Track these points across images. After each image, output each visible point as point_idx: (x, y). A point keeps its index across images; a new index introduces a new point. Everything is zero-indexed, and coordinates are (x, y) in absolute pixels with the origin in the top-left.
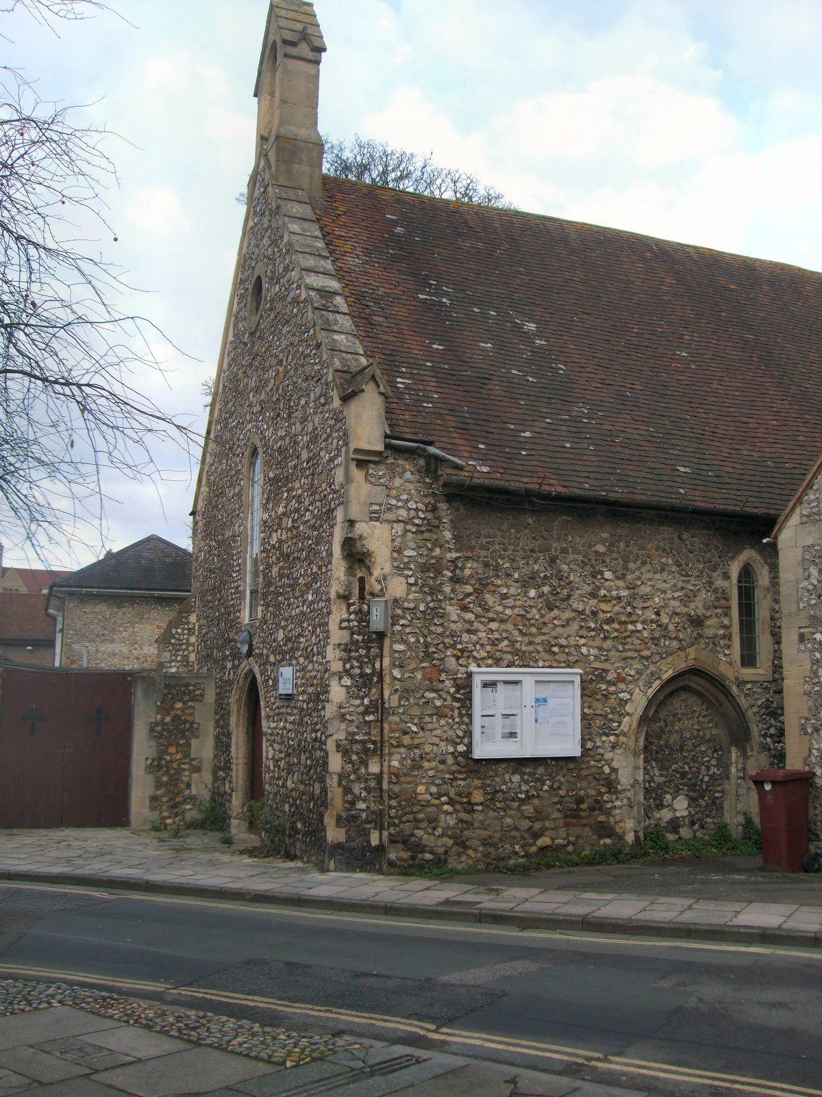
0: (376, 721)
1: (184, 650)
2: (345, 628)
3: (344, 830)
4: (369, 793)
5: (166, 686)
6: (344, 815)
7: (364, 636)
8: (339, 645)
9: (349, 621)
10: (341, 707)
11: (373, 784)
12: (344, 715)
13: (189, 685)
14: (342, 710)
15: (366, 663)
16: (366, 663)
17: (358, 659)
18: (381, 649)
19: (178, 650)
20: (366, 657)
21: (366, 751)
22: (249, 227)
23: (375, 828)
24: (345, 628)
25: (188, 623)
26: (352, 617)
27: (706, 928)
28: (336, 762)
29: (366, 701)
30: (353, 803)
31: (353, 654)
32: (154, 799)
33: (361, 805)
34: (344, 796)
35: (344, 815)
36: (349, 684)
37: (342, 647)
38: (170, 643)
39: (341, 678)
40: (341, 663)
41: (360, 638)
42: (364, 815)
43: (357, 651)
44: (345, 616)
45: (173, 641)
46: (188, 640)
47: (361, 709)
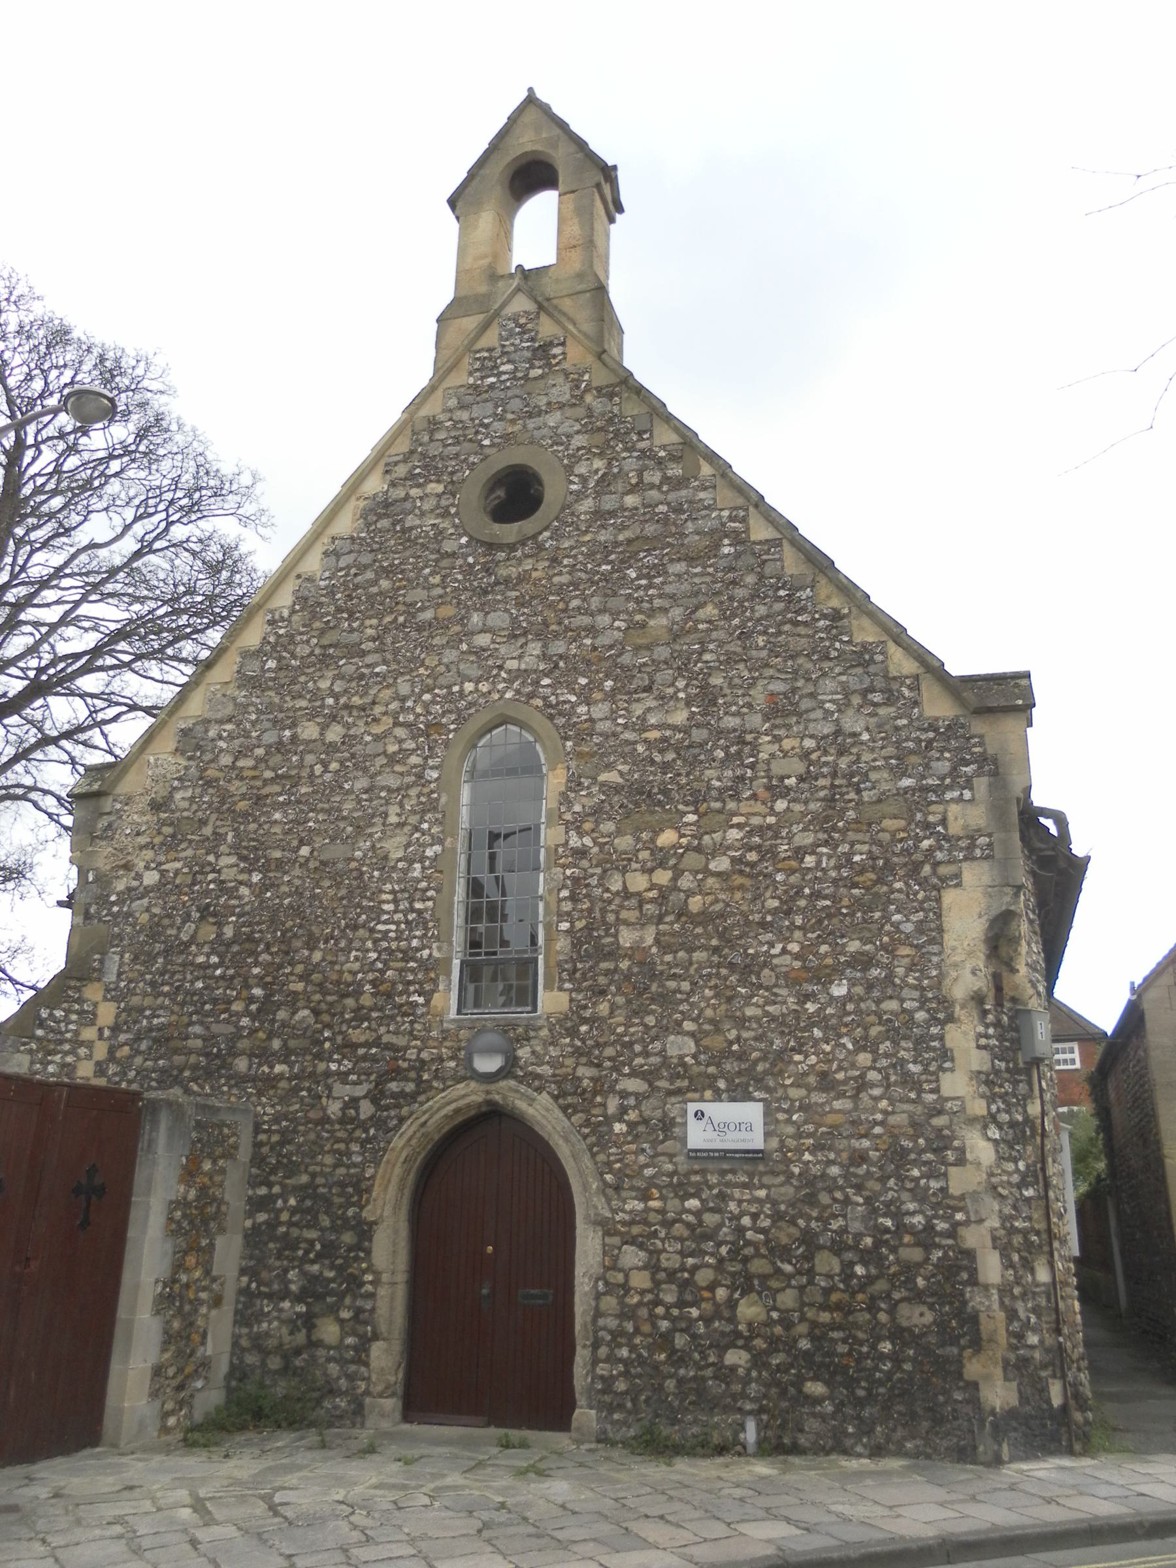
0: (1039, 1198)
1: (66, 1053)
2: (985, 1047)
3: (1014, 1384)
4: (1039, 1317)
5: (199, 1125)
6: (1012, 1357)
7: (1008, 1062)
8: (979, 1072)
9: (987, 1036)
10: (991, 1174)
11: (1043, 1302)
12: (995, 1188)
13: (223, 1124)
14: (994, 1180)
15: (1014, 1105)
16: (1014, 1105)
17: (1003, 1097)
18: (1030, 1084)
19: (54, 1052)
20: (1015, 1096)
21: (1029, 1245)
22: (425, 412)
23: (1054, 1376)
24: (985, 1047)
25: (80, 1001)
26: (991, 1031)
27: (890, 1548)
28: (991, 1268)
29: (1021, 1165)
30: (1020, 1336)
31: (997, 1090)
32: (158, 1371)
33: (1033, 1339)
34: (1008, 1326)
35: (1012, 1357)
36: (997, 1136)
37: (983, 1077)
38: (33, 1037)
39: (985, 1127)
40: (983, 1103)
41: (1003, 1065)
42: (1037, 1355)
43: (1001, 1086)
44: (981, 1029)
45: (40, 1032)
46: (76, 1033)
47: (1016, 1178)
